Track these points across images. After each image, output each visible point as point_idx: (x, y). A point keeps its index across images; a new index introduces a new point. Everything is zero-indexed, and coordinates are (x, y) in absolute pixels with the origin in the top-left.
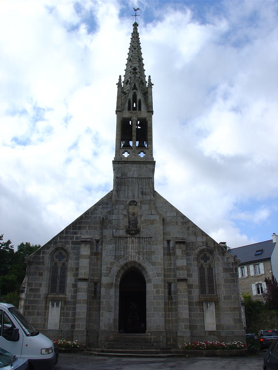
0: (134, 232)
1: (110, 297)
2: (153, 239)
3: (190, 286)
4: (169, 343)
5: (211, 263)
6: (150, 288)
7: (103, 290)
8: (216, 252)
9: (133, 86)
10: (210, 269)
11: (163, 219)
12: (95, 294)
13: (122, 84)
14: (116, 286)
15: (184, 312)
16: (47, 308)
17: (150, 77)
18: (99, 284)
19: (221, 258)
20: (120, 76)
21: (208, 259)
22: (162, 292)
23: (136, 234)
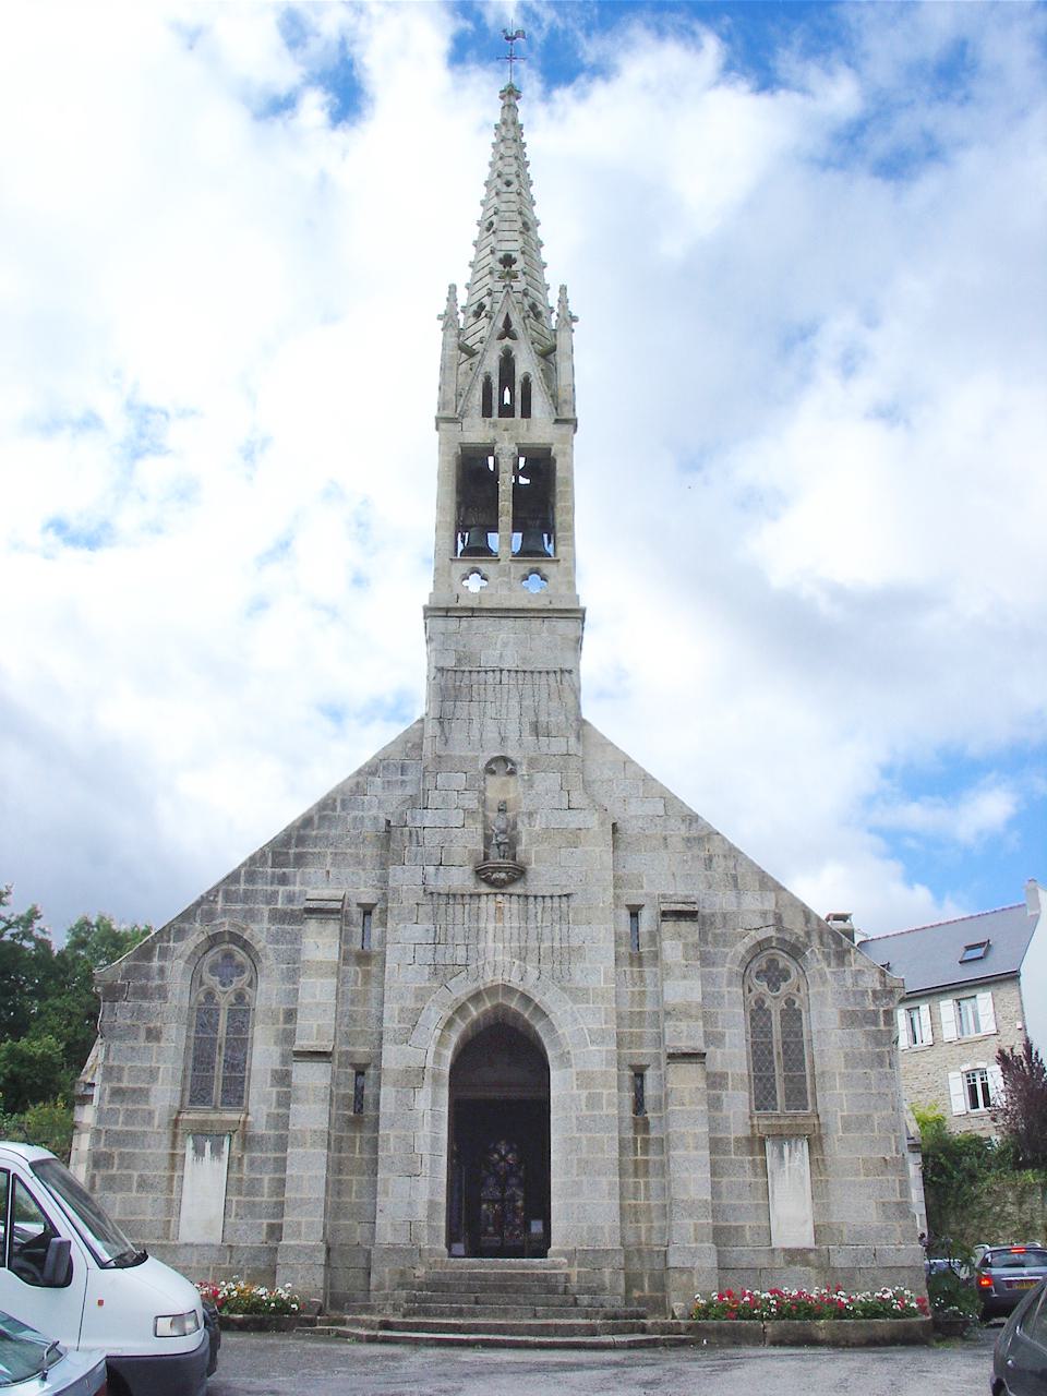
0: (503, 875)
1: (420, 1125)
2: (575, 902)
3: (716, 1081)
4: (636, 1293)
5: (796, 992)
6: (560, 1085)
7: (388, 1094)
8: (814, 953)
9: (500, 324)
10: (792, 1015)
11: (614, 825)
12: (357, 1110)
13: (461, 317)
14: (436, 1078)
15: (691, 1175)
16: (175, 1161)
17: (563, 289)
18: (371, 1071)
19: (834, 973)
20: (453, 289)
21: (785, 975)
22: (614, 1102)
23: (512, 881)
